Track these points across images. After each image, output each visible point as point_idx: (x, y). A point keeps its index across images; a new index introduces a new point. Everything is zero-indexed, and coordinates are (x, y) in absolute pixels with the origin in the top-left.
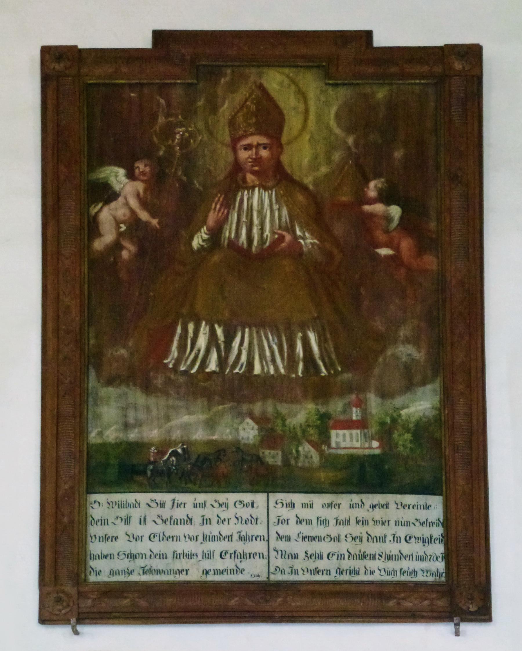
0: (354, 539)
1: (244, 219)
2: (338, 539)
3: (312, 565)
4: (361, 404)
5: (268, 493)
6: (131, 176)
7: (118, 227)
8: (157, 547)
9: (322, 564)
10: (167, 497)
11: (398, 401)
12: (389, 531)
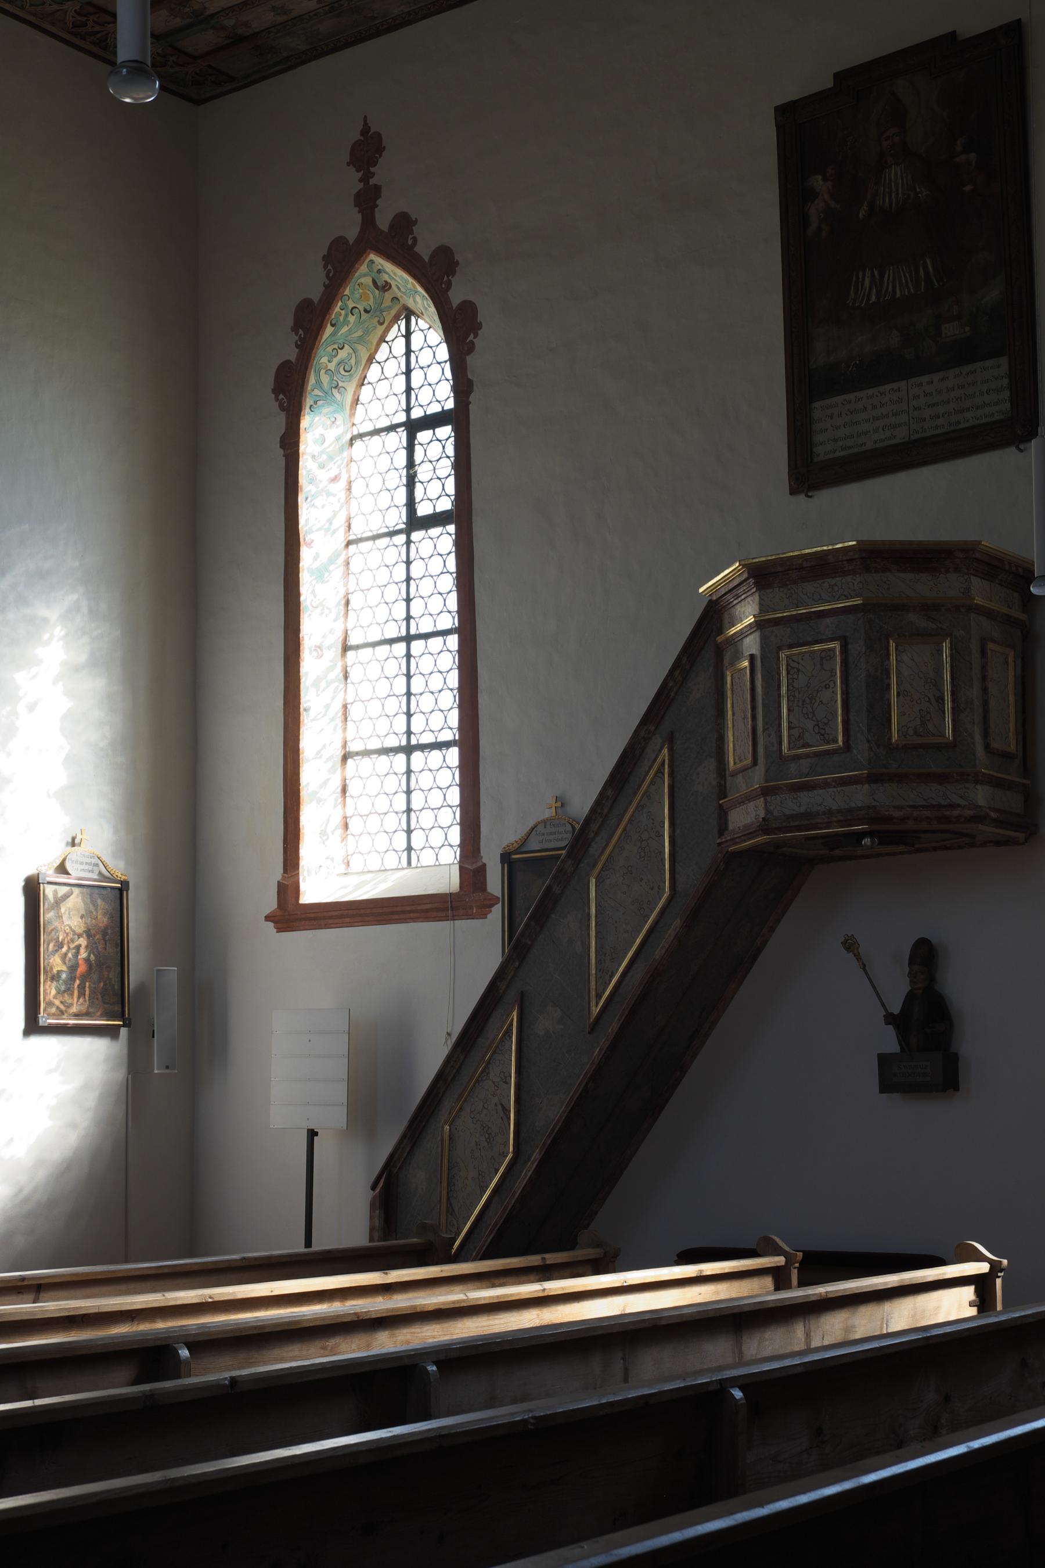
10: (851, 396)
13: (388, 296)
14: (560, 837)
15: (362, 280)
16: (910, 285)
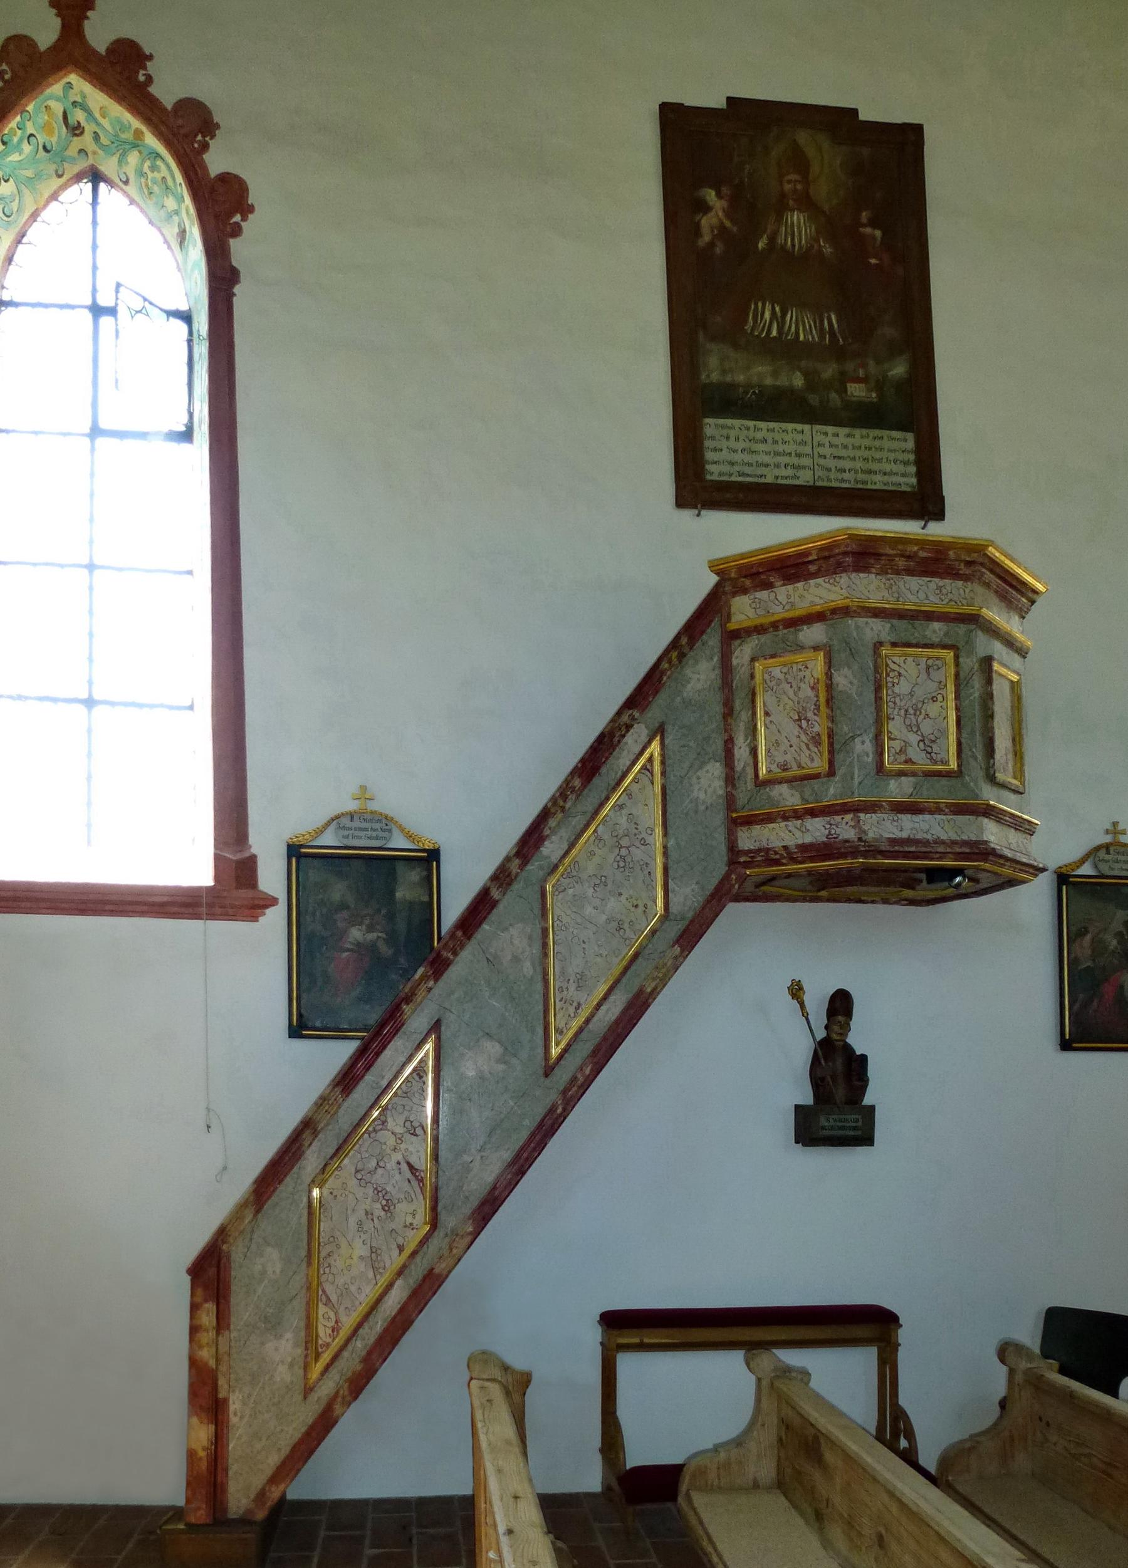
0: (864, 459)
1: (789, 230)
2: (854, 459)
3: (840, 476)
4: (864, 366)
5: (811, 424)
6: (719, 195)
7: (712, 231)
8: (747, 458)
9: (846, 476)
10: (751, 423)
11: (886, 366)
12: (885, 454)
13: (76, 143)
14: (374, 834)
15: (52, 103)
16: (814, 332)
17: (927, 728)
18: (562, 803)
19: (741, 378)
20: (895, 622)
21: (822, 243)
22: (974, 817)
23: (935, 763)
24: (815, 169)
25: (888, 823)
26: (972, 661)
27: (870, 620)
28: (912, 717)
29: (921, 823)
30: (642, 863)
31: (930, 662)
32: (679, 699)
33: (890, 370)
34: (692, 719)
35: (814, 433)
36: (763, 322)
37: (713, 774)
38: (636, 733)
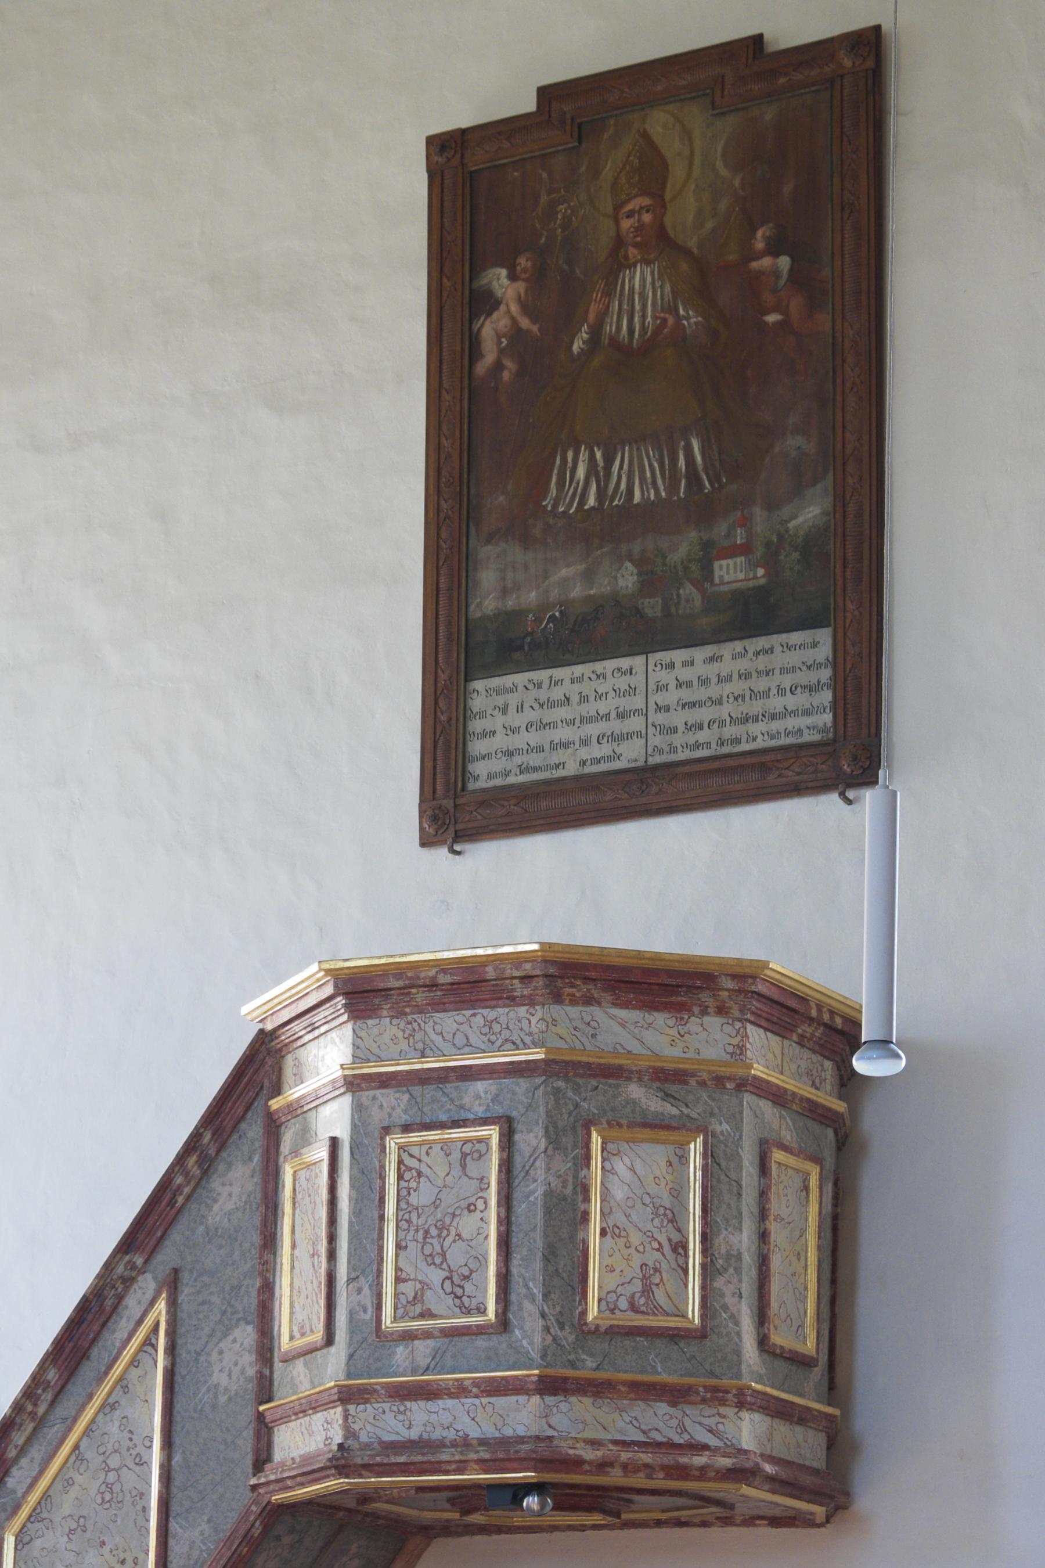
3: (691, 738)
4: (745, 522)
8: (534, 738)
9: (702, 736)
11: (786, 511)
16: (659, 481)
17: (457, 1256)
18: (30, 1408)
19: (531, 597)
20: (417, 1090)
21: (682, 312)
22: (525, 1397)
23: (468, 1312)
24: (677, 172)
25: (389, 1416)
26: (536, 1137)
27: (378, 1092)
28: (435, 1241)
29: (441, 1412)
30: (134, 1493)
31: (467, 1148)
32: (201, 1229)
33: (793, 517)
34: (218, 1260)
35: (651, 667)
36: (574, 485)
37: (242, 1344)
38: (140, 1288)
